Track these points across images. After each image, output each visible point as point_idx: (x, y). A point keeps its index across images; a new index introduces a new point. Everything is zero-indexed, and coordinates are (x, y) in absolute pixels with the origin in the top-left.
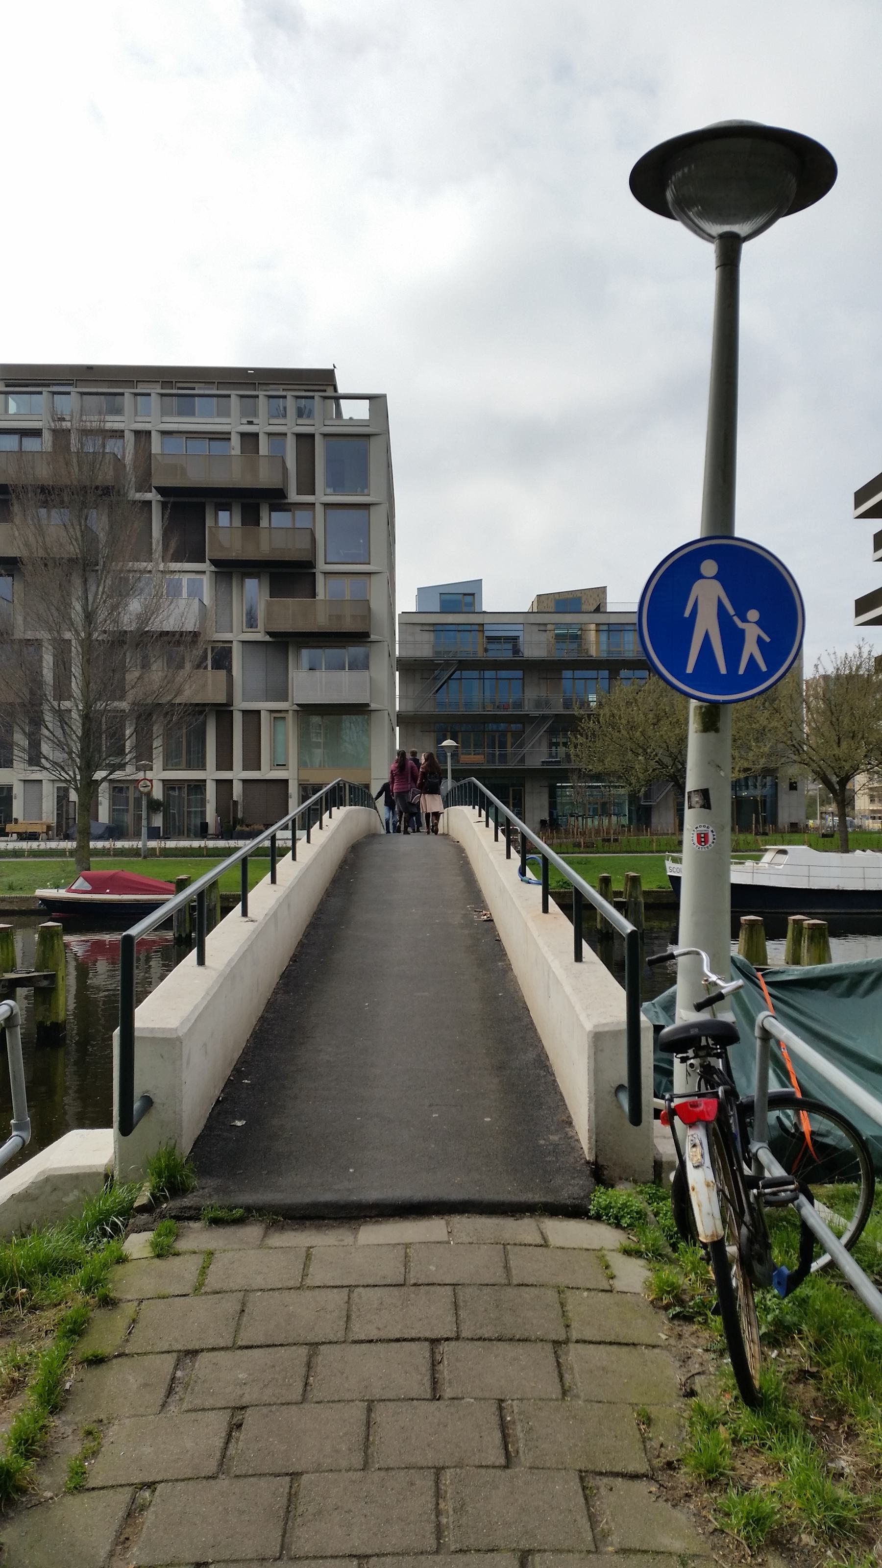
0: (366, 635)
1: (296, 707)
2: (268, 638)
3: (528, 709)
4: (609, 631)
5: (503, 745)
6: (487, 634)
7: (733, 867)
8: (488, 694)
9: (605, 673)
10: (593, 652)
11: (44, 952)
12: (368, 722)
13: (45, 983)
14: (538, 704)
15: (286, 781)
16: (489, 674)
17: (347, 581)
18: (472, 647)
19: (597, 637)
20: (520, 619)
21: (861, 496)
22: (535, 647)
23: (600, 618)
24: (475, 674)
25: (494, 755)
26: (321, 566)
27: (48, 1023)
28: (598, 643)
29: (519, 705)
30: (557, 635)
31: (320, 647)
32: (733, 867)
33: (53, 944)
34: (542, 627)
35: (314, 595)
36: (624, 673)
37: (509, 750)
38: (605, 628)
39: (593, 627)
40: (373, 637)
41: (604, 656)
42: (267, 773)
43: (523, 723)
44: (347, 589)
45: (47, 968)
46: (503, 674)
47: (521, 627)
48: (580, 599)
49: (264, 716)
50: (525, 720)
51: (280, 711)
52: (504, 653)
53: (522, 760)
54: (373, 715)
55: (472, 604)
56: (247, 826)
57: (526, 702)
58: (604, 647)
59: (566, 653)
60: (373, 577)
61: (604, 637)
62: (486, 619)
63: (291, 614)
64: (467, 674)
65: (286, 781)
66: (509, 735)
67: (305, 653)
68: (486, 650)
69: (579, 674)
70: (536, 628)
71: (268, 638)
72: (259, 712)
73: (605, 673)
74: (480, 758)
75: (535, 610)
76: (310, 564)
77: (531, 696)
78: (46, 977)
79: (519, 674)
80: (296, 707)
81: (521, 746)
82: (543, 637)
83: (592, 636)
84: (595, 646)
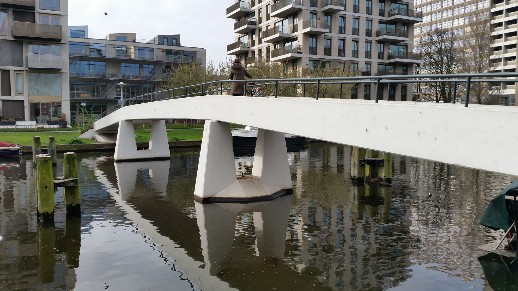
0: (60, 40)
1: (27, 69)
2: (13, 39)
3: (108, 77)
4: (139, 49)
5: (98, 90)
6: (91, 47)
7: (47, 145)
8: (91, 70)
9: (138, 65)
10: (133, 57)
11: (69, 167)
12: (60, 77)
13: (72, 184)
14: (112, 75)
15: (23, 101)
16: (91, 63)
17: (50, 17)
18: (84, 52)
19: (135, 51)
20: (104, 42)
21: (229, 10)
22: (110, 53)
23: (134, 44)
24: (86, 62)
25: (94, 94)
26: (38, 10)
27: (74, 205)
28: (135, 54)
29: (104, 75)
30: (117, 50)
31: (38, 44)
32: (47, 145)
33: (74, 163)
34: (113, 46)
35: (35, 22)
36: (145, 66)
37: (100, 92)
38: (137, 48)
39: (132, 47)
40: (62, 42)
41: (137, 58)
42: (13, 97)
43: (106, 82)
44: (50, 21)
45: (72, 176)
46: (98, 63)
47: (104, 45)
48: (126, 37)
49: (12, 73)
50: (107, 81)
51: (19, 71)
52: (95, 55)
53: (106, 96)
54: (62, 74)
55: (84, 35)
56: (7, 119)
57: (107, 75)
58: (137, 55)
59: (122, 57)
60: (61, 17)
61: (137, 51)
62: (91, 41)
63: (24, 28)
64: (82, 62)
65: (23, 101)
66: (100, 87)
67: (31, 47)
68: (90, 54)
69: (128, 65)
70: (111, 46)
71: (13, 39)
72: (9, 71)
73: (138, 65)
74: (88, 95)
75: (108, 39)
76: (33, 8)
77: (110, 72)
78: (72, 181)
79: (104, 63)
80: (27, 69)
81: (106, 91)
82: (114, 50)
83: (132, 51)
84: (133, 54)
